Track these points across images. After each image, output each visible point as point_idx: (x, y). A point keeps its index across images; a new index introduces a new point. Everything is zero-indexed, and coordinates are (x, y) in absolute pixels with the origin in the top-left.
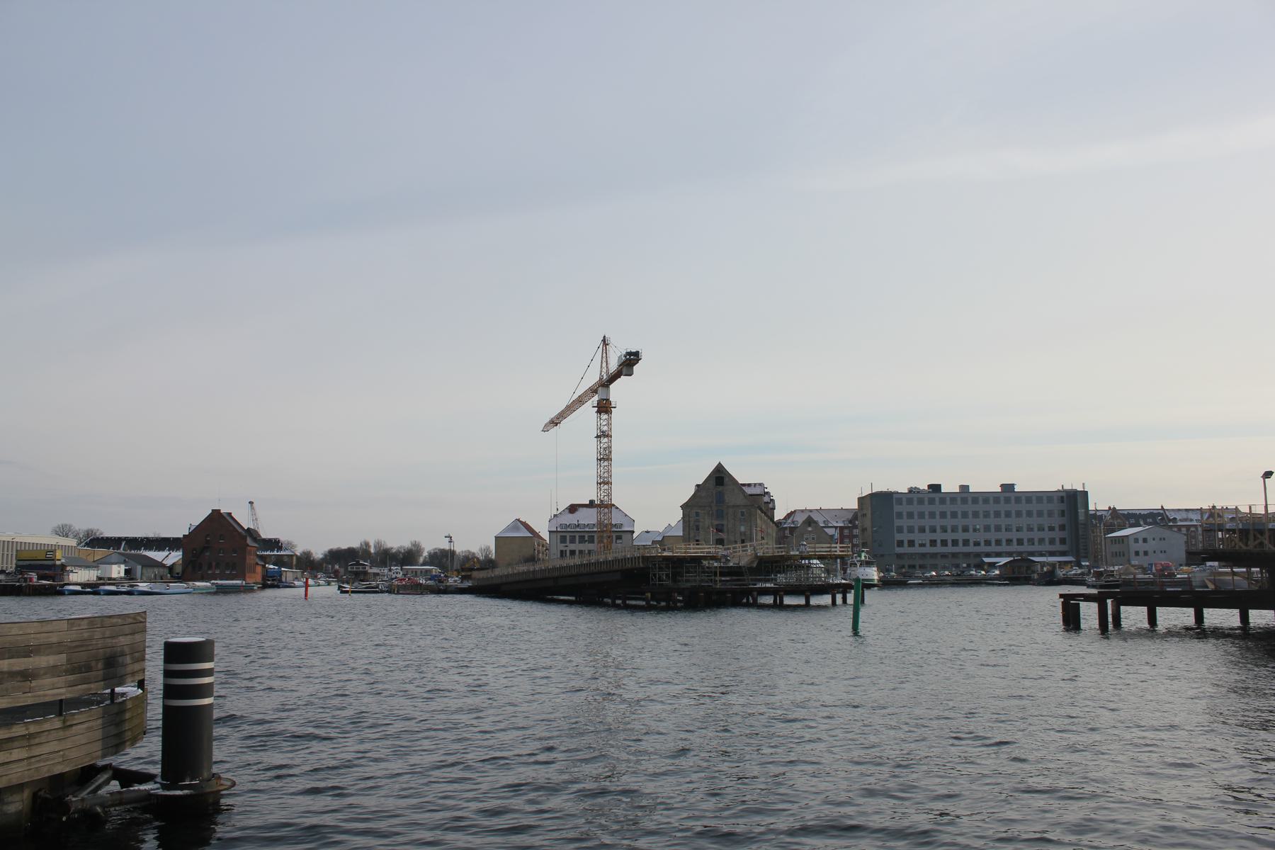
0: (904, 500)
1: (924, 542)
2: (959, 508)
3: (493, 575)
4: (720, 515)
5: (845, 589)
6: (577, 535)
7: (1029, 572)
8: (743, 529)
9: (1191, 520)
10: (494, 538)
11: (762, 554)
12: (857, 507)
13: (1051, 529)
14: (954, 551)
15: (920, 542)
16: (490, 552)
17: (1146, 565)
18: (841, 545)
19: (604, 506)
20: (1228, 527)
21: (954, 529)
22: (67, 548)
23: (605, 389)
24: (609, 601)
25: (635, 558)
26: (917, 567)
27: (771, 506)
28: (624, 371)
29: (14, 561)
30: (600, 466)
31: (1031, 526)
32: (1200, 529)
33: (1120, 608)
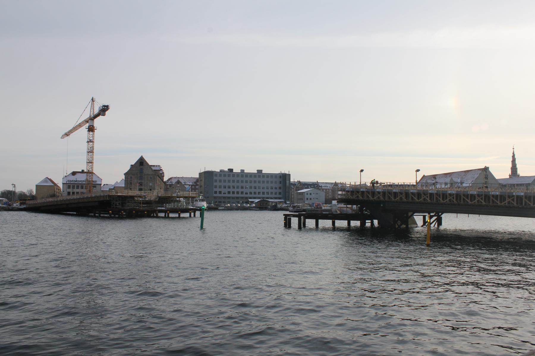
0: (218, 175)
1: (225, 192)
2: (240, 179)
3: (37, 203)
5: (194, 211)
6: (76, 185)
7: (267, 205)
8: (151, 184)
9: (327, 187)
10: (35, 186)
11: (160, 195)
12: (198, 177)
13: (276, 188)
14: (237, 196)
15: (224, 192)
16: (33, 192)
17: (311, 203)
18: (192, 192)
19: (90, 173)
20: (347, 190)
21: (238, 187)
23: (92, 121)
24: (93, 214)
25: (105, 196)
26: (222, 202)
27: (163, 175)
28: (102, 113)
30: (88, 155)
31: (268, 187)
32: (330, 190)
33: (305, 220)
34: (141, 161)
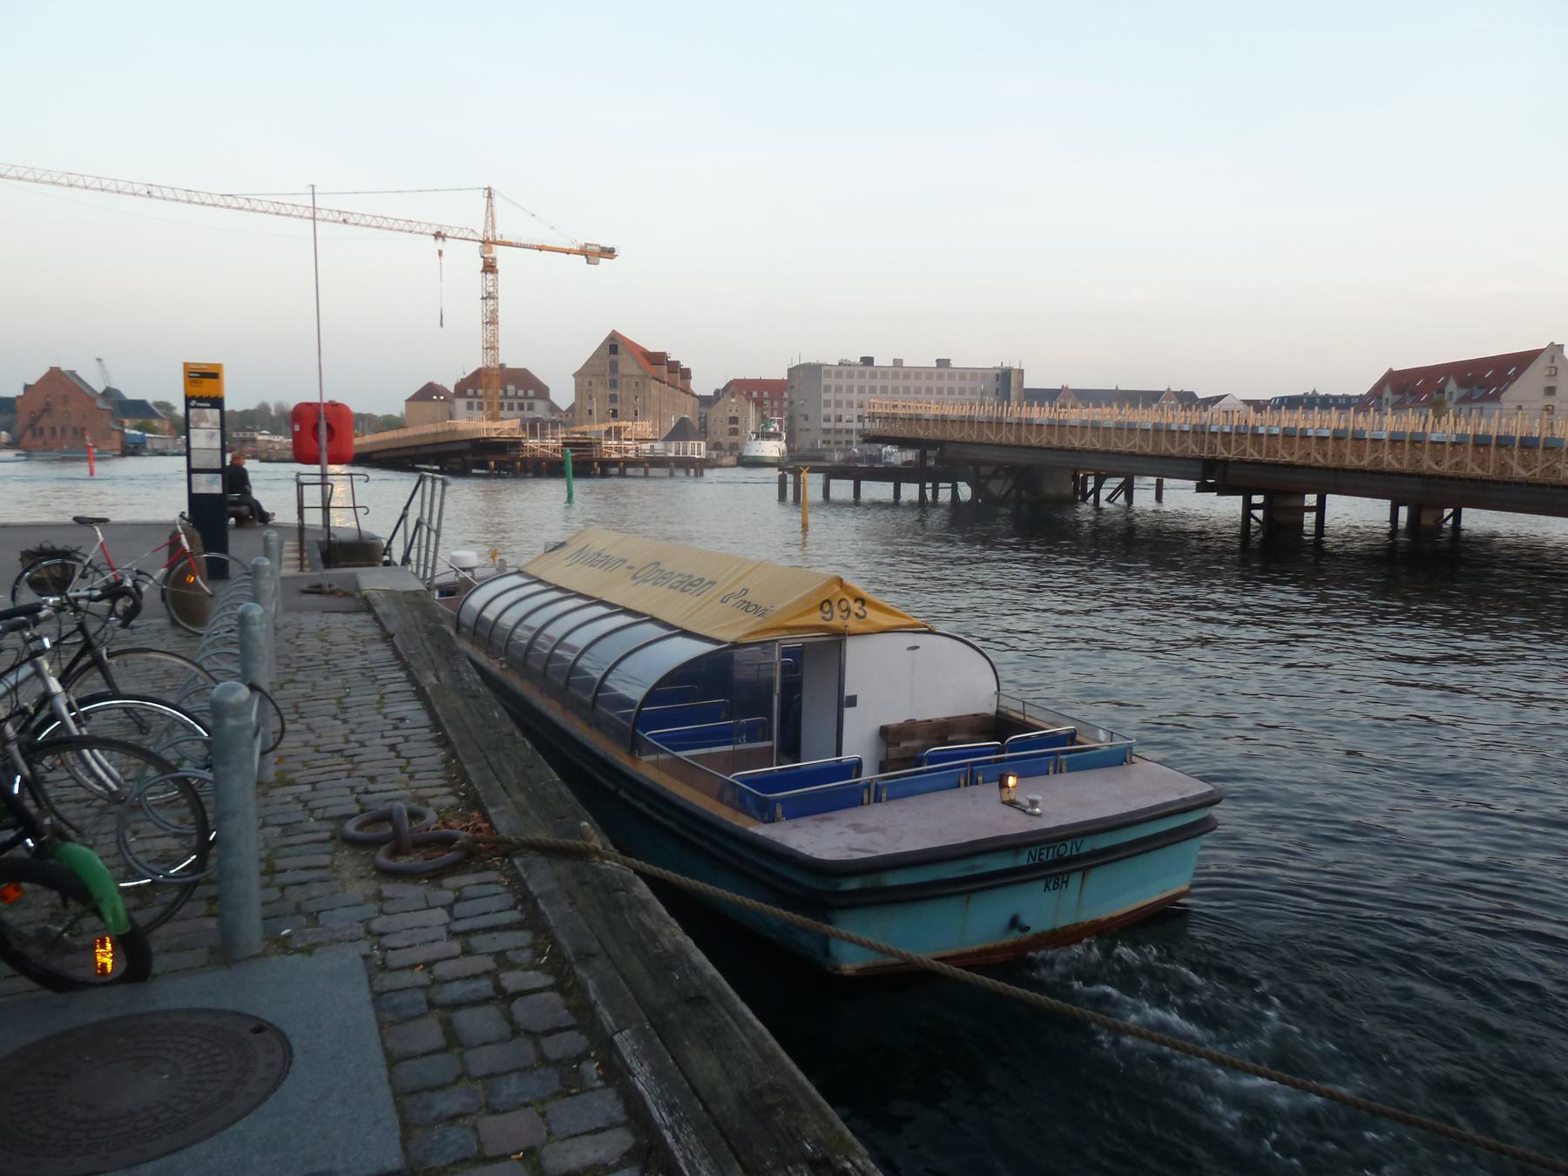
4: (613, 384)
34: (611, 343)
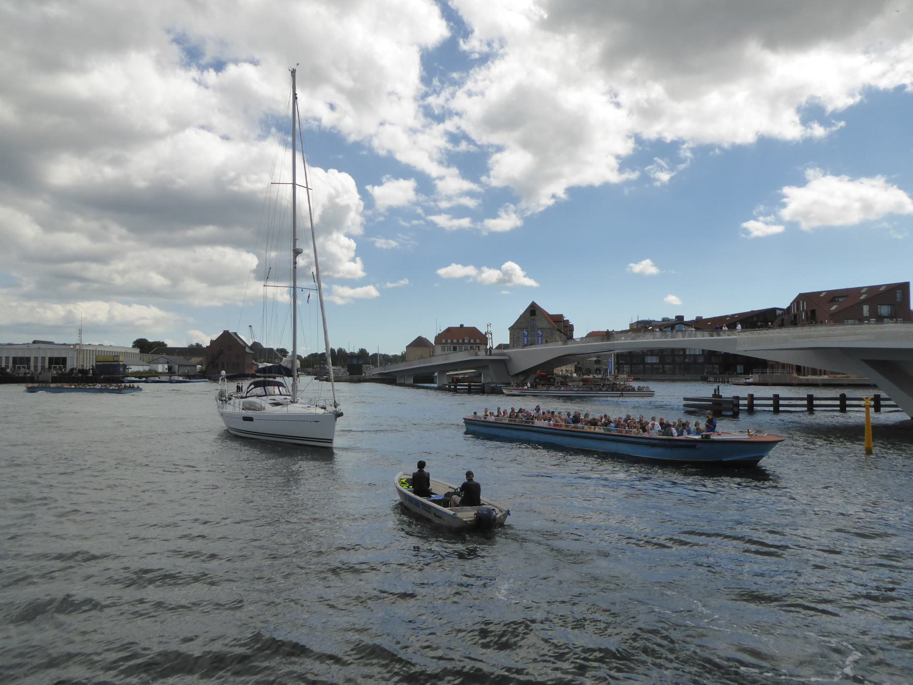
22: (88, 351)
29: (94, 361)
